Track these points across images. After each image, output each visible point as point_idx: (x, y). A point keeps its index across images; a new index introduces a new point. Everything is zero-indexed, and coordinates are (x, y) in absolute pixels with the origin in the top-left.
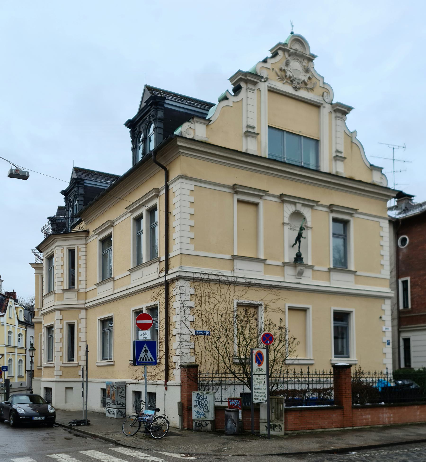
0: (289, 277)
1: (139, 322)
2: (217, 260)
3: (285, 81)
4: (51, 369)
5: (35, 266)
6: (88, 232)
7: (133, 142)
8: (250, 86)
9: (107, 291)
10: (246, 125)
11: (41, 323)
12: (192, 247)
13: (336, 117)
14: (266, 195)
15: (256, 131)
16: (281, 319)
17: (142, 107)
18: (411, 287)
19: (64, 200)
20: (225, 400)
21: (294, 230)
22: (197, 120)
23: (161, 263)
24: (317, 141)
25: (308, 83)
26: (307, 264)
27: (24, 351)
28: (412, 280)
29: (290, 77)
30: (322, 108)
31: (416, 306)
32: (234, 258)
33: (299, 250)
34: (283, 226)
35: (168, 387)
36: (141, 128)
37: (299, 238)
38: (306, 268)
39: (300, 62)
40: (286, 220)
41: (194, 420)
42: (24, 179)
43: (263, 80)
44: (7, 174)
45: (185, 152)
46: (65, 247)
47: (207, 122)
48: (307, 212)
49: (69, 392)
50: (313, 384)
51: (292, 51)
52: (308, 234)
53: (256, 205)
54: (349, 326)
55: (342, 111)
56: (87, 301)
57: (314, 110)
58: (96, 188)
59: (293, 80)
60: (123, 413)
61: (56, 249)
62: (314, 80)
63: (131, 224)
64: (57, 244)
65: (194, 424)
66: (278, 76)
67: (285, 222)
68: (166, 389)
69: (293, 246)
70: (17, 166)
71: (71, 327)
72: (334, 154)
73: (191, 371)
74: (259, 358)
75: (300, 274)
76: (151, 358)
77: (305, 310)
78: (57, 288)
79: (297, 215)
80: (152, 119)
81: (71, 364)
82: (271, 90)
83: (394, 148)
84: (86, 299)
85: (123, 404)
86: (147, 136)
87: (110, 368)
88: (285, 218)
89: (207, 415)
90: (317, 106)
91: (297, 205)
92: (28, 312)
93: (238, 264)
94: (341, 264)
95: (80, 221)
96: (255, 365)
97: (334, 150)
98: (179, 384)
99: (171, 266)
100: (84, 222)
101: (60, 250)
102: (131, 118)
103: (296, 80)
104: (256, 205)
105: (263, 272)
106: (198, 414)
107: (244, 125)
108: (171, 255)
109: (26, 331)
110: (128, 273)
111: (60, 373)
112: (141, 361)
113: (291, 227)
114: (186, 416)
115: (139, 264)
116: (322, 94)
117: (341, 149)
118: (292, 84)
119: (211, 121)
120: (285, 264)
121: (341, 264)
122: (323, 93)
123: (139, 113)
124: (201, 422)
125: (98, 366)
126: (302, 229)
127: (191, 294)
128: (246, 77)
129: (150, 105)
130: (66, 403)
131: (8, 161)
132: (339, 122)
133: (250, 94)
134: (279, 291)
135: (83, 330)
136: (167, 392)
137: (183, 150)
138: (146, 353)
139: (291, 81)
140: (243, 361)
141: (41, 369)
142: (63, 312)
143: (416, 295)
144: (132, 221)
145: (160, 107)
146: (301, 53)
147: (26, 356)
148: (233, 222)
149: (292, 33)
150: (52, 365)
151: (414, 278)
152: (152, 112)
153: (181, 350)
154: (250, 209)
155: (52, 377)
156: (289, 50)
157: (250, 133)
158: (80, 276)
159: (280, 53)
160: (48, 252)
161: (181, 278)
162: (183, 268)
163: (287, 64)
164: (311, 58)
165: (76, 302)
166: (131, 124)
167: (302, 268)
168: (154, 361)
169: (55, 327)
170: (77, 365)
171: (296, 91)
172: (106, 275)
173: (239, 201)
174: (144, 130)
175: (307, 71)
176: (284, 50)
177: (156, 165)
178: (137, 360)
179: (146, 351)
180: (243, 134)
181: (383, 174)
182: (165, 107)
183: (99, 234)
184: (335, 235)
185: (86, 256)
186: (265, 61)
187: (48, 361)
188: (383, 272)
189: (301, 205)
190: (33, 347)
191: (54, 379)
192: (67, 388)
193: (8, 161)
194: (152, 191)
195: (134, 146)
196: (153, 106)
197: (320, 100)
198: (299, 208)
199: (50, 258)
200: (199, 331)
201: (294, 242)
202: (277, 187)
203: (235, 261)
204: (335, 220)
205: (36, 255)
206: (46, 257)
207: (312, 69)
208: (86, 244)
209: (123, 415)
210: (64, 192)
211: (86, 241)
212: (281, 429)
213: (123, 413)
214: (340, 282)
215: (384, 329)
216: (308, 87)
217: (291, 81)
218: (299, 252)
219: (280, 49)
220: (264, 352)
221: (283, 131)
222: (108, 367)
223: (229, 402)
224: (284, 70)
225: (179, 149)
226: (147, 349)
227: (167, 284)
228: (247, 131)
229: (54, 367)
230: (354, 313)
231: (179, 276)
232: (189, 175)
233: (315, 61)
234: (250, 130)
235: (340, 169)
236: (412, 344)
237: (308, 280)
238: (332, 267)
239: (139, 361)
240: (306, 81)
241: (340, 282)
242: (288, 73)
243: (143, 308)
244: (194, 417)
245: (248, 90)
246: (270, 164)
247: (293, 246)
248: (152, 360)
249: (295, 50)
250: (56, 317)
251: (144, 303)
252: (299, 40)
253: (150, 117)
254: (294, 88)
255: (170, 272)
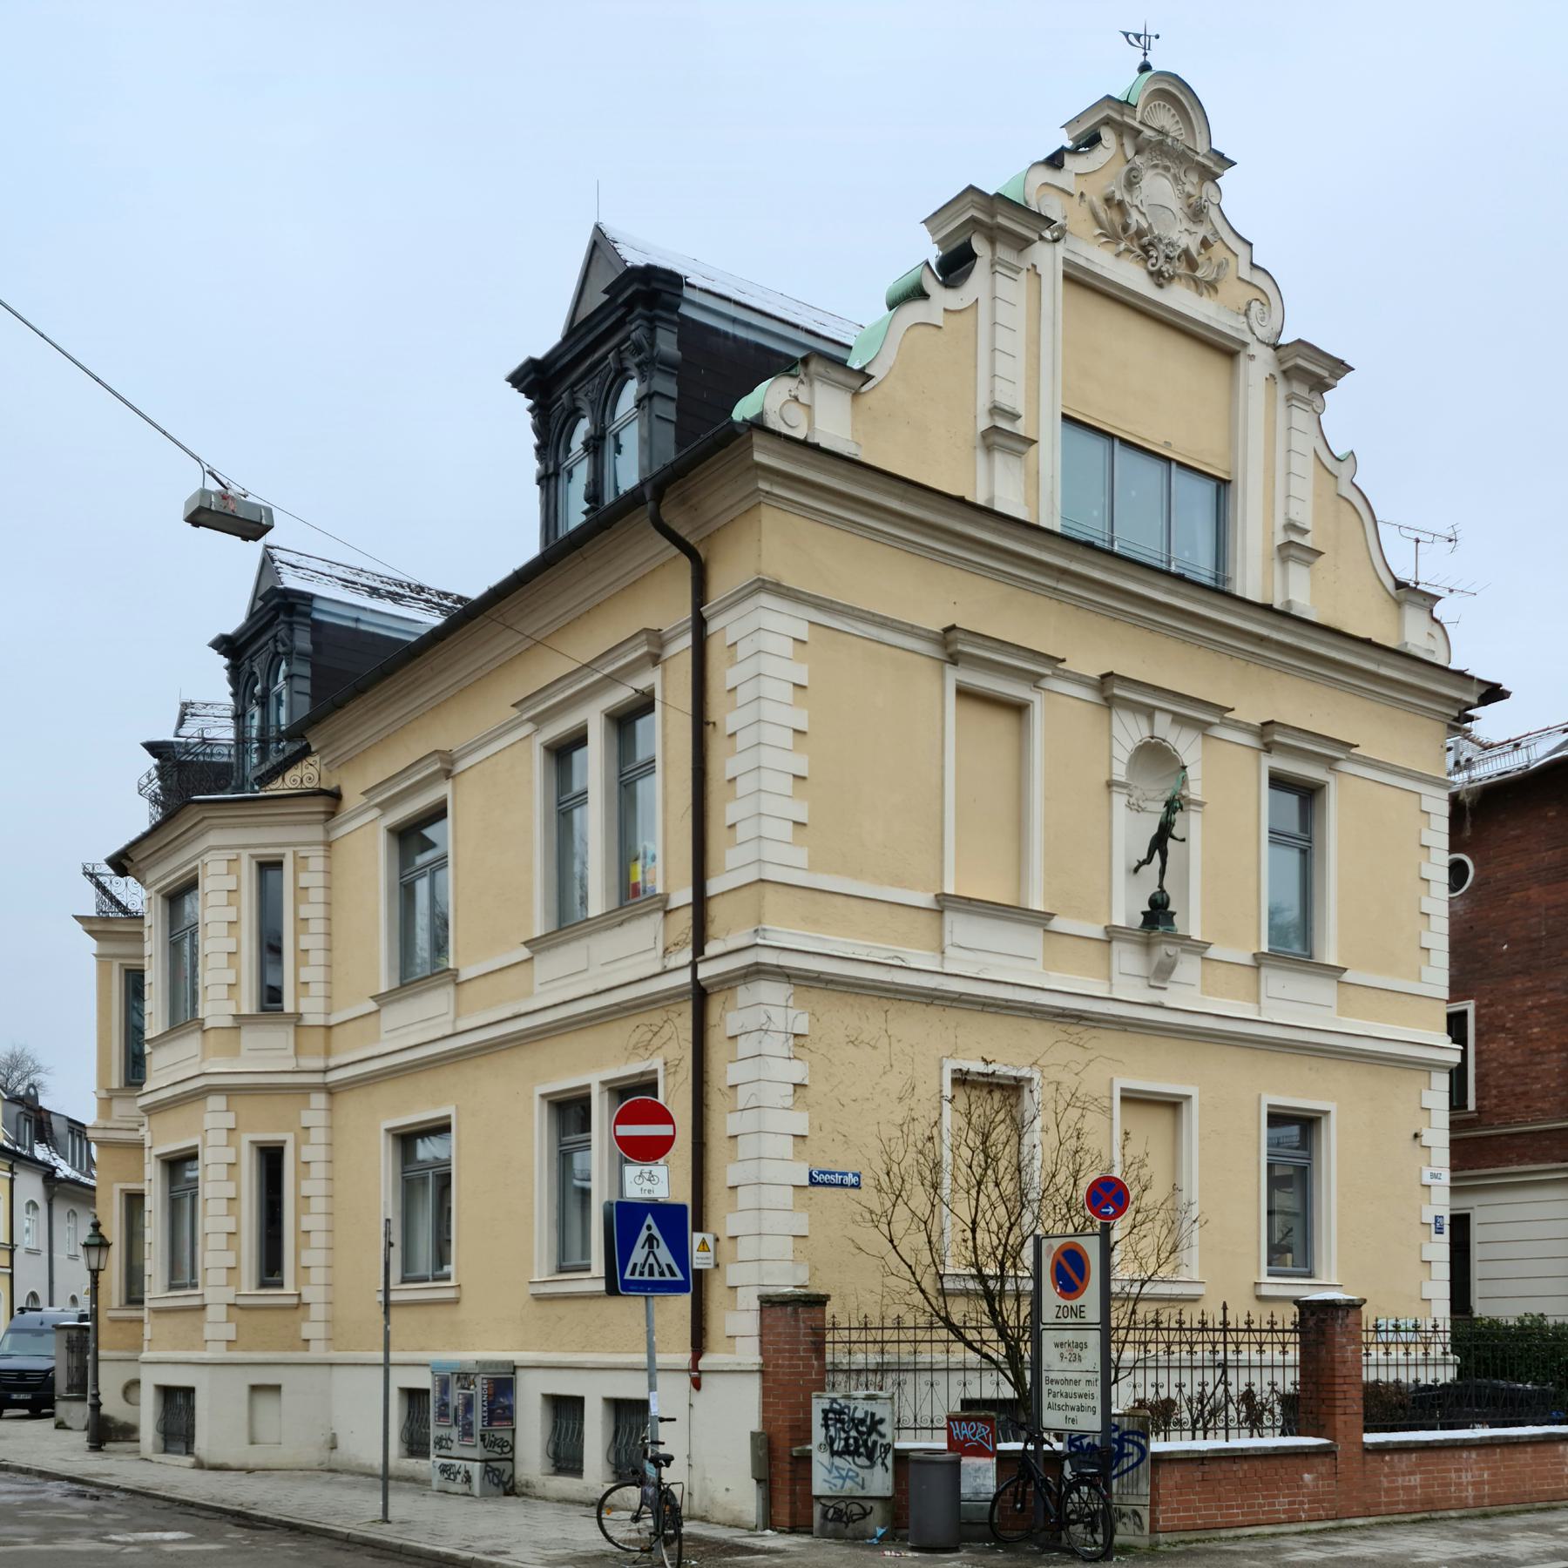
0: (1123, 982)
1: (624, 1130)
2: (885, 907)
3: (1122, 246)
4: (190, 1318)
5: (96, 927)
6: (335, 796)
7: (541, 451)
8: (1004, 253)
9: (425, 1020)
10: (988, 405)
11: (139, 1146)
12: (800, 856)
13: (1290, 398)
14: (1055, 676)
15: (1020, 428)
16: (1127, 1133)
17: (585, 311)
18: (1479, 1035)
19: (225, 674)
20: (928, 1424)
21: (1140, 810)
22: (821, 370)
23: (672, 917)
24: (1222, 485)
25: (1200, 260)
26: (1189, 937)
27: (6, 1255)
28: (1483, 1011)
29: (1140, 234)
30: (1242, 358)
31: (1495, 1101)
32: (945, 903)
33: (1161, 886)
34: (1110, 793)
35: (705, 1379)
36: (580, 395)
37: (1160, 841)
38: (1183, 951)
39: (1176, 179)
40: (1120, 772)
41: (818, 1498)
42: (246, 538)
43: (1047, 234)
44: (180, 512)
45: (777, 491)
46: (245, 854)
47: (856, 383)
48: (1187, 746)
49: (265, 1403)
50: (1192, 1368)
51: (1148, 133)
52: (1191, 825)
53: (1019, 709)
54: (1315, 1165)
55: (1311, 373)
56: (333, 1062)
57: (1213, 366)
58: (356, 631)
59: (1151, 244)
60: (505, 1478)
61: (206, 858)
62: (1218, 251)
63: (536, 764)
64: (213, 838)
65: (817, 1510)
66: (1100, 224)
67: (1115, 777)
68: (697, 1384)
69: (1136, 870)
70: (225, 481)
71: (271, 1159)
72: (1280, 539)
73: (796, 1316)
74: (1071, 1271)
75: (1163, 972)
76: (669, 1266)
77: (1173, 1105)
78: (214, 1007)
79: (1154, 754)
80: (631, 362)
81: (271, 1296)
82: (1078, 279)
83: (1417, 541)
84: (328, 1053)
85: (502, 1444)
86: (604, 429)
87: (440, 1314)
88: (1115, 763)
89: (868, 1478)
90: (1227, 350)
91: (1158, 716)
92: (17, 1109)
93: (959, 927)
94: (1294, 945)
95: (305, 752)
96: (1052, 1298)
97: (1280, 521)
98: (756, 1368)
99: (713, 929)
100: (317, 758)
101: (222, 863)
102: (539, 354)
103: (1162, 247)
104: (1019, 709)
105: (1040, 960)
106: (835, 1473)
107: (983, 404)
108: (714, 886)
109: (12, 1180)
110: (525, 953)
111: (230, 1331)
112: (637, 1277)
113: (1132, 800)
114: (782, 1485)
115: (567, 922)
116: (1244, 308)
117: (1304, 517)
118: (1146, 261)
119: (870, 377)
120: (1113, 934)
121: (1294, 945)
122: (1249, 304)
123: (566, 338)
124: (842, 1505)
125: (539, 1298)
126: (1174, 805)
127: (796, 1035)
128: (993, 216)
129: (624, 303)
130: (252, 1443)
131: (193, 456)
132: (1300, 417)
133: (1004, 285)
134: (1095, 1032)
135: (318, 1170)
136: (698, 1398)
137: (772, 483)
138: (651, 1246)
139: (1145, 246)
140: (991, 1284)
141: (141, 1321)
142: (238, 1101)
143: (1495, 1064)
144: (537, 757)
145: (664, 314)
146: (1180, 147)
147: (11, 1275)
148: (943, 767)
149: (1145, 68)
150: (196, 1302)
151: (1490, 1005)
152: (636, 331)
153: (761, 1241)
154: (1000, 723)
155: (192, 1347)
156: (1140, 132)
157: (1002, 438)
158: (307, 964)
159: (1108, 135)
160: (169, 871)
161: (759, 972)
162: (768, 935)
163: (1131, 182)
164: (1214, 166)
165: (290, 1065)
166: (535, 379)
167: (1171, 950)
168: (680, 1277)
169: (206, 1156)
170: (295, 1300)
171: (1160, 286)
172: (421, 960)
173: (963, 693)
174: (592, 402)
175: (1197, 213)
176: (1121, 129)
177: (658, 536)
178: (622, 1274)
179: (651, 1239)
180: (978, 441)
181: (1436, 621)
182: (682, 316)
183: (384, 806)
184: (1277, 837)
185: (327, 888)
186: (1055, 161)
187: (172, 1287)
188: (1428, 974)
189: (1169, 718)
190: (102, 1236)
191: (206, 1355)
192: (255, 1389)
193: (193, 456)
194: (637, 641)
195: (547, 467)
196: (639, 310)
197: (1237, 330)
198: (1164, 728)
199: (178, 896)
200: (824, 1173)
201: (1144, 856)
202: (1093, 647)
203: (948, 915)
204: (1279, 782)
205: (99, 885)
206: (158, 892)
207: (1213, 213)
208: (328, 845)
209: (505, 1484)
210: (225, 645)
211: (327, 832)
212: (1141, 1527)
213: (505, 1478)
214: (1293, 1004)
215: (1427, 1180)
216: (1199, 274)
217: (1145, 246)
218: (1162, 891)
219: (1107, 122)
220: (1091, 1248)
221: (1111, 436)
222: (432, 1309)
223: (949, 1430)
224: (1120, 204)
225: (756, 478)
226: (655, 1232)
227: (700, 995)
228: (995, 429)
229: (203, 1307)
230: (1333, 1117)
231: (757, 964)
232: (789, 582)
233: (1227, 179)
234: (1004, 424)
235: (1301, 592)
236: (1477, 1234)
237: (1191, 994)
238: (1265, 948)
239: (627, 1276)
240: (1194, 251)
241: (1293, 1004)
242: (1135, 218)
243: (588, 1086)
244: (820, 1486)
245: (998, 268)
246: (1072, 558)
247: (1136, 870)
248: (673, 1274)
249: (1154, 128)
250: (209, 1120)
251: (594, 1068)
252: (1175, 94)
253: (621, 352)
254: (1151, 274)
255: (710, 950)
